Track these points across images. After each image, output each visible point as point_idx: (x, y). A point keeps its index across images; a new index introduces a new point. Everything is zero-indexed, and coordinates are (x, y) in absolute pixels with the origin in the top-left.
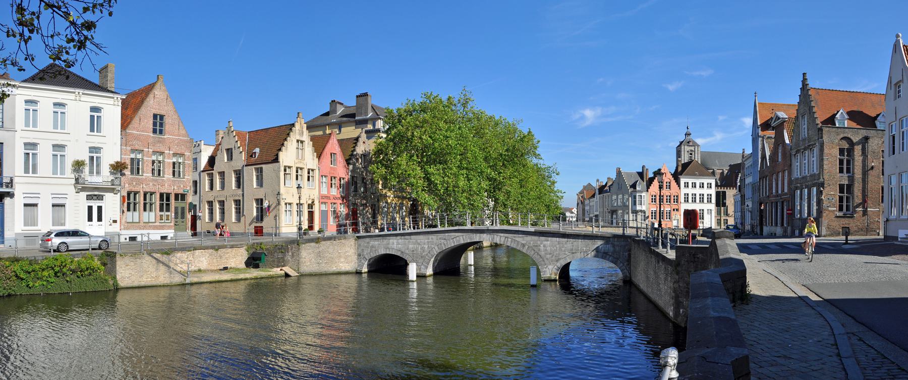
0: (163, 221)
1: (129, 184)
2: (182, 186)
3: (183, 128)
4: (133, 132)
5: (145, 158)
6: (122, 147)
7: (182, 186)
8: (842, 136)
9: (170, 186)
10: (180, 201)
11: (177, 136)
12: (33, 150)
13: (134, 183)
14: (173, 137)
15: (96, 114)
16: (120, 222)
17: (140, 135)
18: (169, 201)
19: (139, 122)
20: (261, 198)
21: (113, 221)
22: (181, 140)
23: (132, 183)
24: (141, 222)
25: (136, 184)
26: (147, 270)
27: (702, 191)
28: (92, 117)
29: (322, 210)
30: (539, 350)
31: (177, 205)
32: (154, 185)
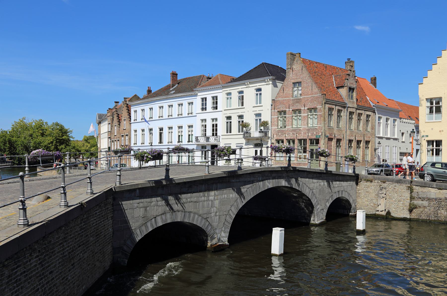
1: (276, 135)
2: (315, 133)
7: (315, 133)
8: (211, 79)
9: (305, 133)
10: (315, 145)
11: (311, 94)
20: (305, 138)
23: (279, 134)
27: (180, 122)
30: (333, 263)
31: (312, 148)
32: (293, 134)
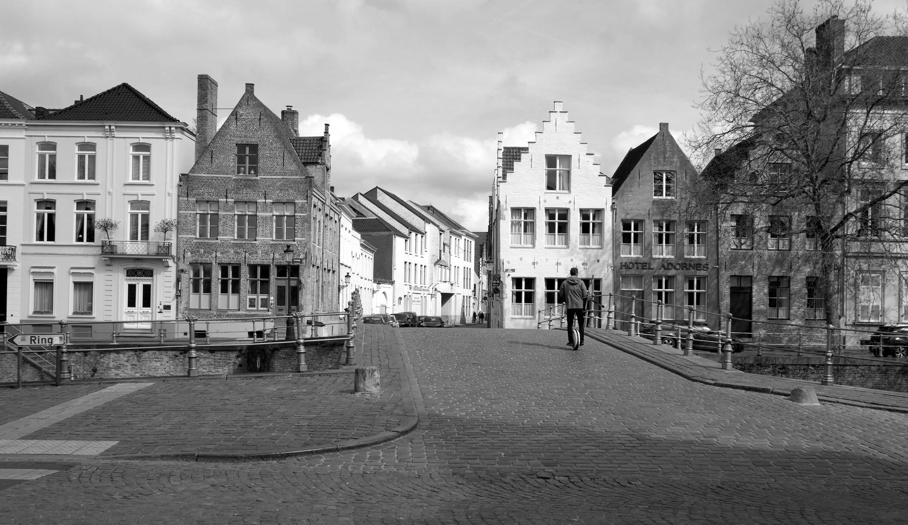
0: (255, 309)
3: (291, 161)
4: (199, 175)
5: (221, 213)
6: (181, 198)
9: (266, 253)
11: (280, 174)
12: (49, 208)
13: (202, 251)
14: (273, 177)
15: (87, 153)
16: (177, 307)
17: (212, 178)
19: (210, 159)
21: (164, 306)
23: (198, 251)
24: (213, 308)
25: (205, 252)
26: (9, 371)
28: (81, 158)
29: (292, 287)
31: (283, 283)
32: (236, 253)
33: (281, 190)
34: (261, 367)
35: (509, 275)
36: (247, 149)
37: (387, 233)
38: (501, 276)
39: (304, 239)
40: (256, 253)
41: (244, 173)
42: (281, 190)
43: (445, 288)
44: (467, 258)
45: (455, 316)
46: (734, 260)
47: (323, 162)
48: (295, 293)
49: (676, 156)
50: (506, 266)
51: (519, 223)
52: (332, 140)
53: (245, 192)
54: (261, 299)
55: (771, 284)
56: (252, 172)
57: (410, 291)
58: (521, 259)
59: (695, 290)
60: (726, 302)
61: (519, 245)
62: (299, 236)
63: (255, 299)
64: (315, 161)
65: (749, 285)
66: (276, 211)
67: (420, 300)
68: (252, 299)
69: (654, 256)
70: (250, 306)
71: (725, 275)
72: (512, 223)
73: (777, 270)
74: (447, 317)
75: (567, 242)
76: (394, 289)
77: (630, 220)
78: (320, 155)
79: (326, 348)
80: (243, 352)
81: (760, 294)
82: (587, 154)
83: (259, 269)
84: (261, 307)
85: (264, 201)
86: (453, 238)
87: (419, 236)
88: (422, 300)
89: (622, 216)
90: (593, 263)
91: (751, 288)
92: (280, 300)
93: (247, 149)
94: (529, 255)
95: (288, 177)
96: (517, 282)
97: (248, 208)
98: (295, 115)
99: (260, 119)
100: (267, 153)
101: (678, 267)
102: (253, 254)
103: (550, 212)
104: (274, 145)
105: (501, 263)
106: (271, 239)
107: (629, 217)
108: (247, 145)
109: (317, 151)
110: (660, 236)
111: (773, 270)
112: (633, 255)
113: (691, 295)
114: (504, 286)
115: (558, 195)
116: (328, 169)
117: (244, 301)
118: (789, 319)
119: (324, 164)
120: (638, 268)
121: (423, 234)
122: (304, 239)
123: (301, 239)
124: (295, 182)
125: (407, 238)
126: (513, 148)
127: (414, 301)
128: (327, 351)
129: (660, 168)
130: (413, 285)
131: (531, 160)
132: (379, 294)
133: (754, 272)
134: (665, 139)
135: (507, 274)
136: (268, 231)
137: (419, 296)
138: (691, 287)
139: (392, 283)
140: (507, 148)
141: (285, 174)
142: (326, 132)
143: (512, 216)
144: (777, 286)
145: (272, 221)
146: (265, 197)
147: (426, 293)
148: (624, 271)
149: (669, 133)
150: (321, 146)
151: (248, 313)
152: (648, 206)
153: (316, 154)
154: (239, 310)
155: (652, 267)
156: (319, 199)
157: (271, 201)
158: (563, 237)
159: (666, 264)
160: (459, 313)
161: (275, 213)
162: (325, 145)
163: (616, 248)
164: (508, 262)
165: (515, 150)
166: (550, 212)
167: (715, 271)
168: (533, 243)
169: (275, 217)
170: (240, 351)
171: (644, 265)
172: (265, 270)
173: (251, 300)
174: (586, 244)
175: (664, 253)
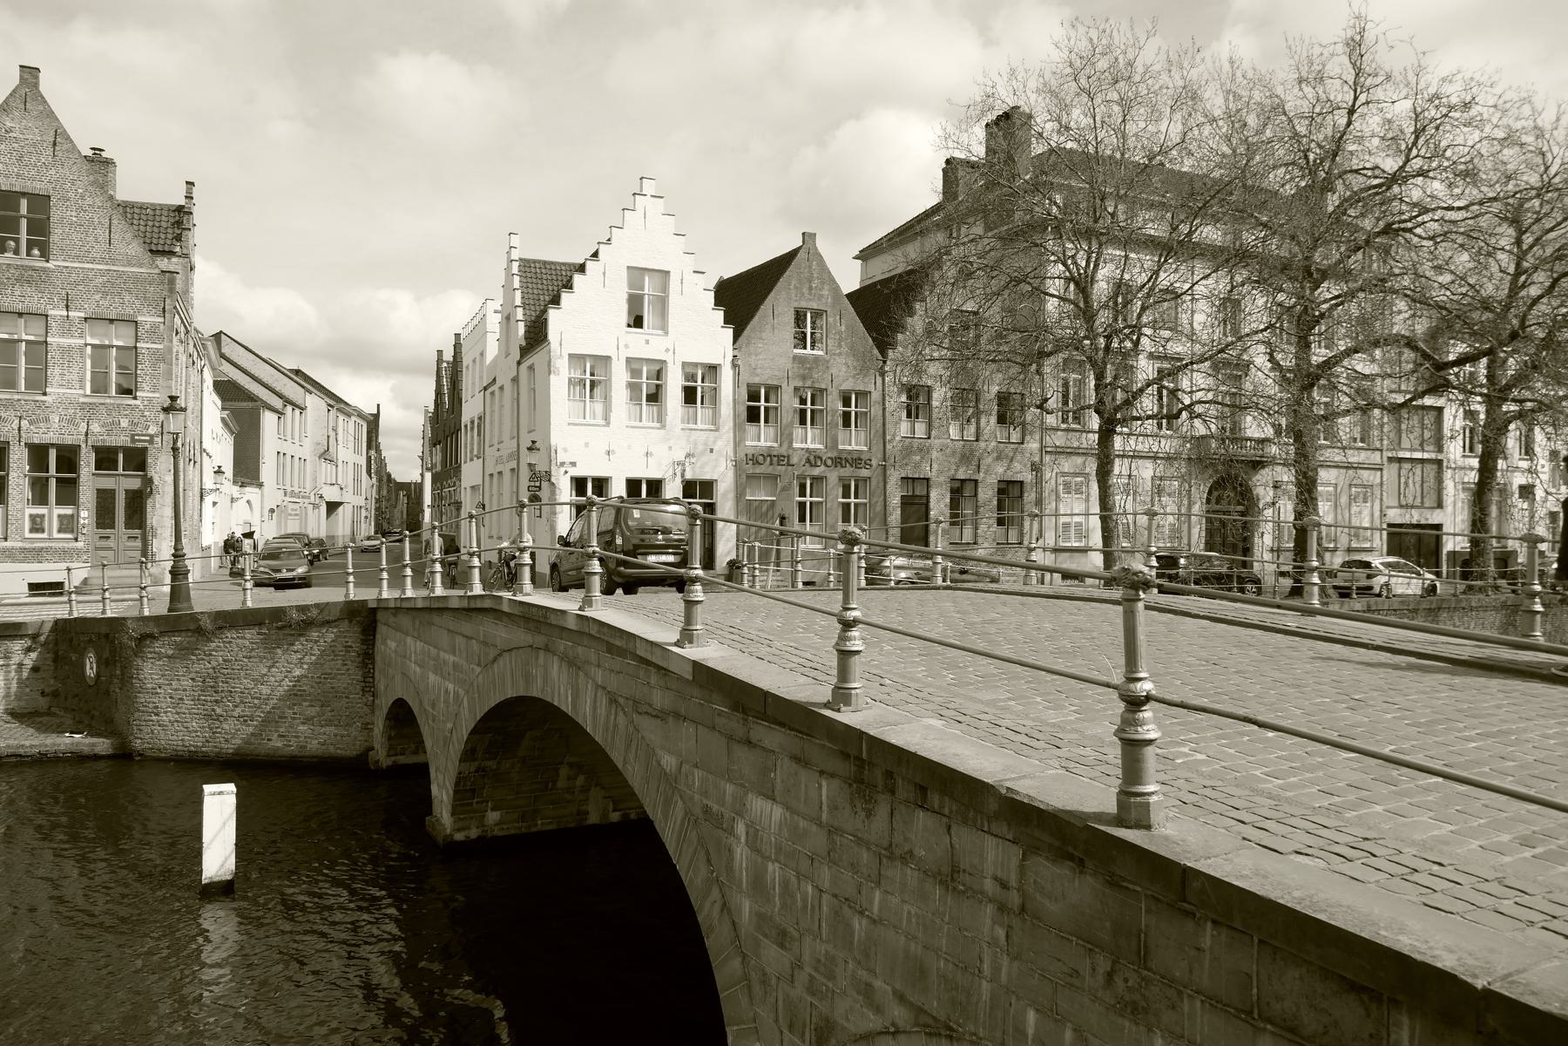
0: (45, 535)
2: (124, 423)
3: (129, 236)
9: (71, 421)
10: (120, 471)
11: (102, 261)
14: (86, 266)
18: (749, 408)
22: (120, 274)
31: (107, 483)
33: (105, 294)
34: (98, 675)
35: (566, 472)
36: (24, 203)
37: (251, 404)
38: (553, 473)
39: (157, 395)
40: (47, 420)
41: (16, 252)
42: (105, 294)
43: (332, 495)
44: (357, 451)
45: (344, 536)
46: (908, 451)
47: (185, 251)
48: (137, 504)
49: (826, 287)
50: (561, 457)
51: (582, 382)
52: (199, 216)
53: (18, 293)
54: (59, 516)
55: (953, 491)
56: (36, 252)
57: (285, 499)
58: (587, 445)
59: (852, 500)
60: (895, 517)
61: (581, 420)
62: (147, 388)
63: (44, 516)
64: (167, 249)
65: (925, 493)
66: (92, 336)
67: (298, 512)
68: (38, 516)
69: (795, 445)
70: (32, 530)
71: (894, 477)
72: (570, 380)
73: (961, 470)
74: (333, 537)
75: (661, 418)
76: (262, 495)
77: (759, 386)
78: (178, 238)
79: (287, 631)
80: (42, 638)
81: (939, 504)
82: (695, 272)
83: (53, 454)
84: (59, 531)
85: (65, 313)
86: (341, 417)
87: (297, 411)
88: (301, 511)
89: (746, 378)
90: (703, 453)
91: (928, 496)
92: (104, 516)
93: (24, 203)
94: (600, 438)
95: (121, 269)
96: (579, 484)
97: (25, 327)
98: (111, 168)
99: (55, 144)
100: (72, 215)
101: (829, 462)
102: (38, 421)
103: (633, 365)
104: (89, 201)
105: (553, 451)
106: (81, 392)
107: (757, 380)
108: (24, 194)
109: (170, 231)
110: (803, 413)
111: (956, 470)
112: (762, 443)
113: (846, 507)
114: (558, 492)
115: (647, 337)
116: (191, 269)
117: (17, 520)
118: (975, 543)
119: (186, 256)
120: (771, 464)
121: (302, 409)
122: (157, 395)
123: (151, 395)
124: (136, 279)
125: (280, 413)
126: (535, 261)
127: (290, 515)
128: (290, 638)
129: (804, 304)
130: (289, 489)
131: (604, 273)
132: (242, 503)
133: (932, 475)
134: (811, 258)
135: (563, 470)
136: (75, 377)
137: (297, 506)
138: (846, 494)
139: (261, 485)
140: (528, 261)
141: (113, 261)
142: (189, 197)
143: (570, 370)
144: (960, 491)
145: (82, 356)
146: (67, 307)
147: (307, 501)
148: (750, 469)
149: (816, 249)
150: (179, 223)
151: (27, 545)
152: (785, 363)
153: (170, 236)
154: (6, 539)
155: (791, 462)
156: (182, 322)
157: (82, 315)
158: (655, 408)
159: (812, 458)
160: (348, 532)
161: (90, 340)
162: (188, 221)
163: (738, 428)
164: (565, 450)
165: (537, 265)
166: (633, 365)
167: (880, 470)
168: (607, 419)
169: (89, 348)
170: (35, 637)
171: (781, 459)
172: (68, 458)
173: (33, 518)
174: (691, 421)
175: (808, 440)
